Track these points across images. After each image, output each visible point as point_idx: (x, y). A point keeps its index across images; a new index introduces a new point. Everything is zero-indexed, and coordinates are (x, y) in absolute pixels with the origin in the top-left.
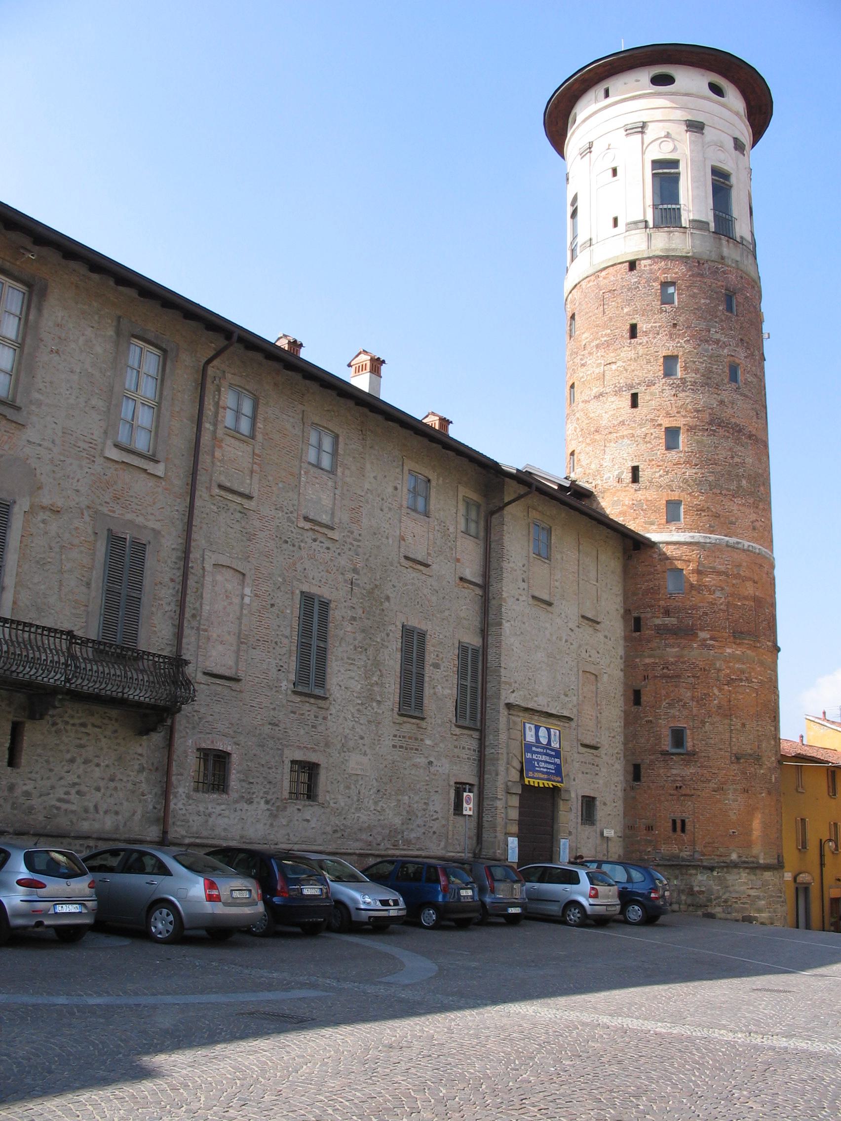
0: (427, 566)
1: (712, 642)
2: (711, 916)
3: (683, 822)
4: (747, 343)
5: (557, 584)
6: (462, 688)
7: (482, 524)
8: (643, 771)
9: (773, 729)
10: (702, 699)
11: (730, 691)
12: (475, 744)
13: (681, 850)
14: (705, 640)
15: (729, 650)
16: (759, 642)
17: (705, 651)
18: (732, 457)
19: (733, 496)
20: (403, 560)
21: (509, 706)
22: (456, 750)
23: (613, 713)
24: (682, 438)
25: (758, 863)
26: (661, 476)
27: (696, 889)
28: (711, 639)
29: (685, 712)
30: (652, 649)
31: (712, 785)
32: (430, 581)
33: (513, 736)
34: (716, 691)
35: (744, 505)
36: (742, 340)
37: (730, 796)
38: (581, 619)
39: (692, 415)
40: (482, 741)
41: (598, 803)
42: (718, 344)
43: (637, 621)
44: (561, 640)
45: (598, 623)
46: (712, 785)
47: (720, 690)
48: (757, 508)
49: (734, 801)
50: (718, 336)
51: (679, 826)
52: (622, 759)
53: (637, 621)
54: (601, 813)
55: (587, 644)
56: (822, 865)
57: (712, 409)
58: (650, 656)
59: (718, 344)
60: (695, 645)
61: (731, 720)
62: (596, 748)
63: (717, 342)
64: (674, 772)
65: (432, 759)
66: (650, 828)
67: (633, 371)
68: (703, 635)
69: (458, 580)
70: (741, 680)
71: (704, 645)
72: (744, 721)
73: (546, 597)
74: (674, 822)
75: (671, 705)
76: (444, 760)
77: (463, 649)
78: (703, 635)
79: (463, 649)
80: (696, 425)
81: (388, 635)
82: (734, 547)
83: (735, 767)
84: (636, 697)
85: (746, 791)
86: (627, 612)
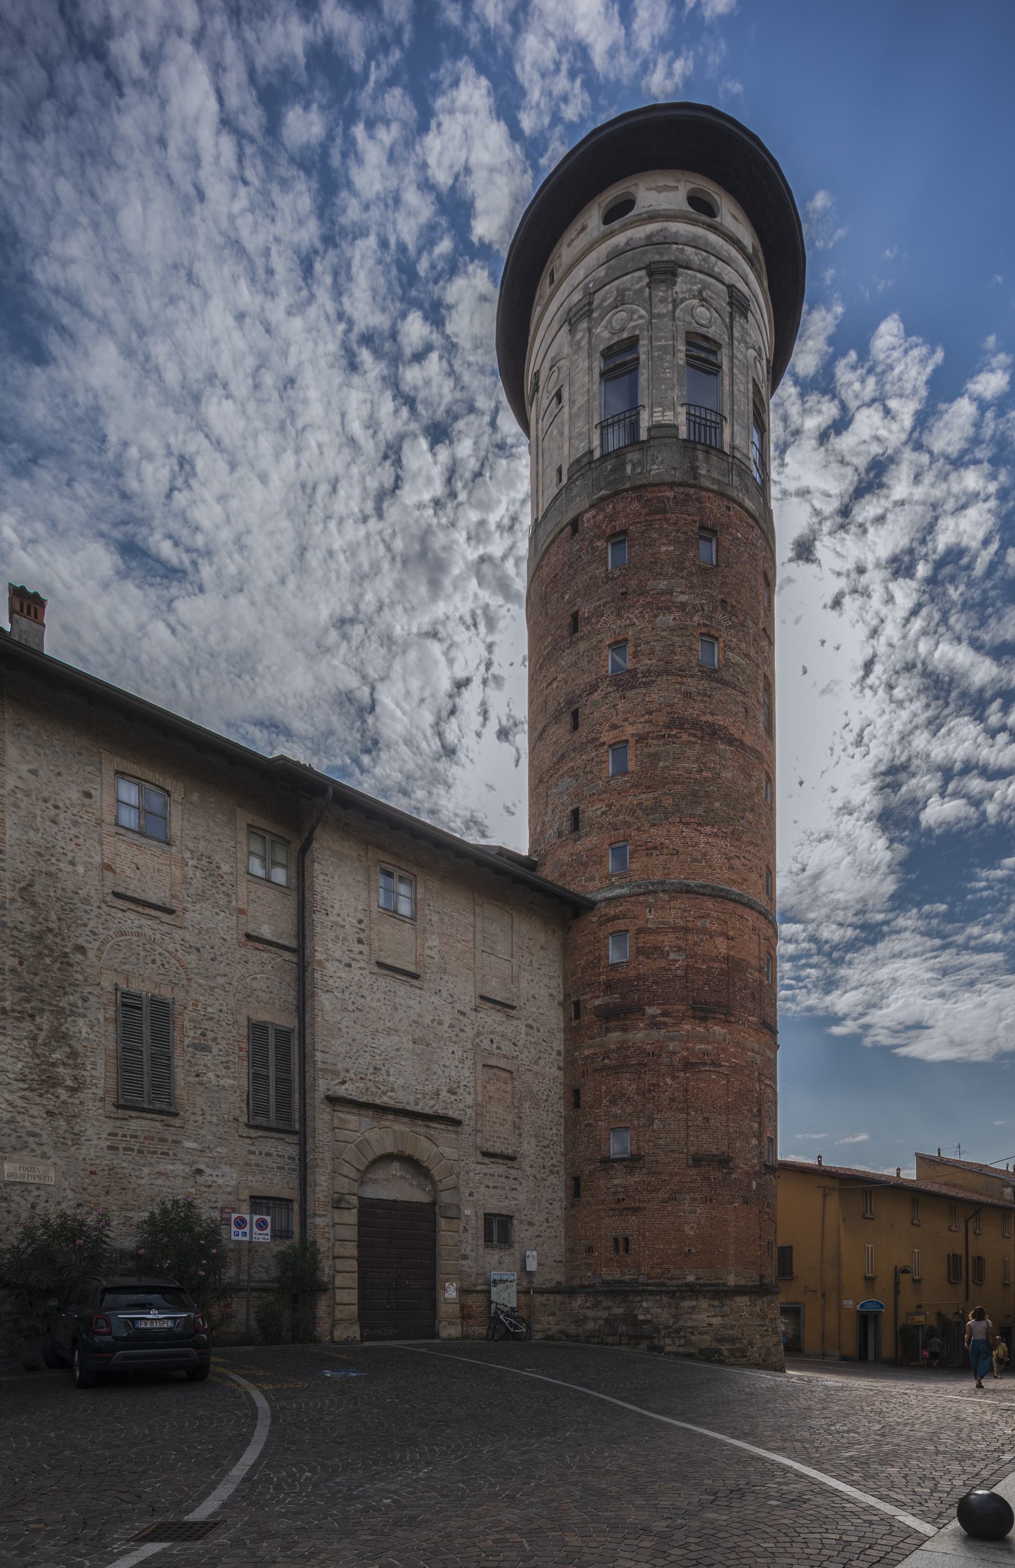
0: (171, 912)
1: (662, 1019)
2: (660, 1349)
3: (626, 1240)
4: (733, 606)
5: (432, 953)
6: (258, 1079)
7: (293, 867)
8: (583, 1184)
9: (756, 1125)
10: (650, 1091)
11: (687, 1079)
12: (293, 1151)
13: (623, 1273)
14: (654, 1017)
15: (688, 1027)
16: (732, 1015)
17: (654, 1032)
18: (700, 771)
19: (700, 824)
20: (109, 898)
21: (334, 1101)
22: (252, 1157)
23: (548, 1116)
24: (631, 753)
25: (725, 1284)
26: (603, 813)
27: (641, 1317)
28: (664, 1014)
29: (629, 1109)
30: (592, 1038)
31: (661, 1195)
32: (178, 934)
33: (343, 1141)
34: (669, 1080)
35: (716, 835)
36: (723, 601)
37: (687, 1207)
38: (479, 1000)
39: (642, 720)
40: (303, 1145)
41: (515, 1222)
42: (684, 610)
43: (577, 1004)
44: (440, 1023)
45: (513, 1008)
46: (661, 1195)
47: (674, 1078)
48: (738, 840)
49: (691, 1212)
50: (683, 598)
51: (622, 1244)
52: (562, 1173)
53: (577, 1004)
54: (520, 1232)
55: (492, 1033)
56: (897, 1292)
57: (672, 705)
58: (589, 1047)
59: (684, 610)
60: (642, 1025)
61: (688, 1114)
62: (513, 1159)
63: (683, 606)
64: (616, 1182)
65: (202, 1167)
66: (590, 1250)
67: (573, 679)
68: (650, 1011)
69: (243, 939)
70: (704, 1064)
71: (654, 1024)
72: (706, 1115)
73: (411, 968)
74: (616, 1240)
75: (613, 1102)
76: (226, 1169)
77: (257, 1030)
78: (650, 1011)
79: (257, 1030)
80: (648, 733)
81: (85, 1000)
82: (698, 893)
83: (694, 1171)
84: (575, 1098)
85: (706, 1200)
86: (567, 996)
